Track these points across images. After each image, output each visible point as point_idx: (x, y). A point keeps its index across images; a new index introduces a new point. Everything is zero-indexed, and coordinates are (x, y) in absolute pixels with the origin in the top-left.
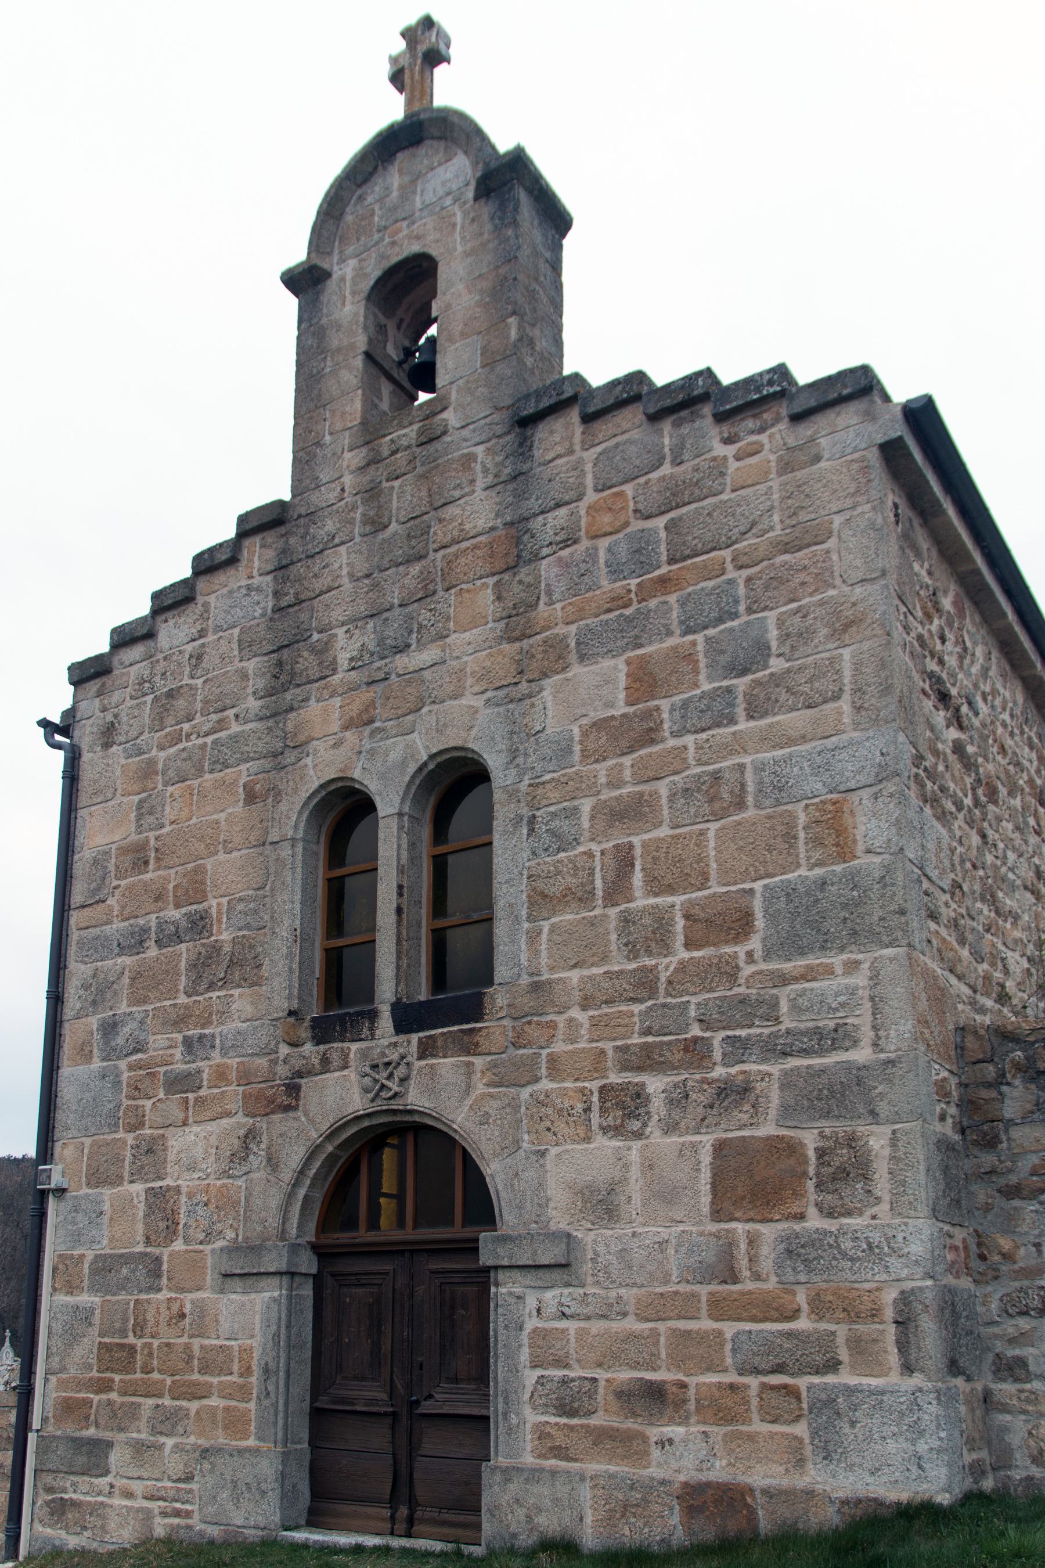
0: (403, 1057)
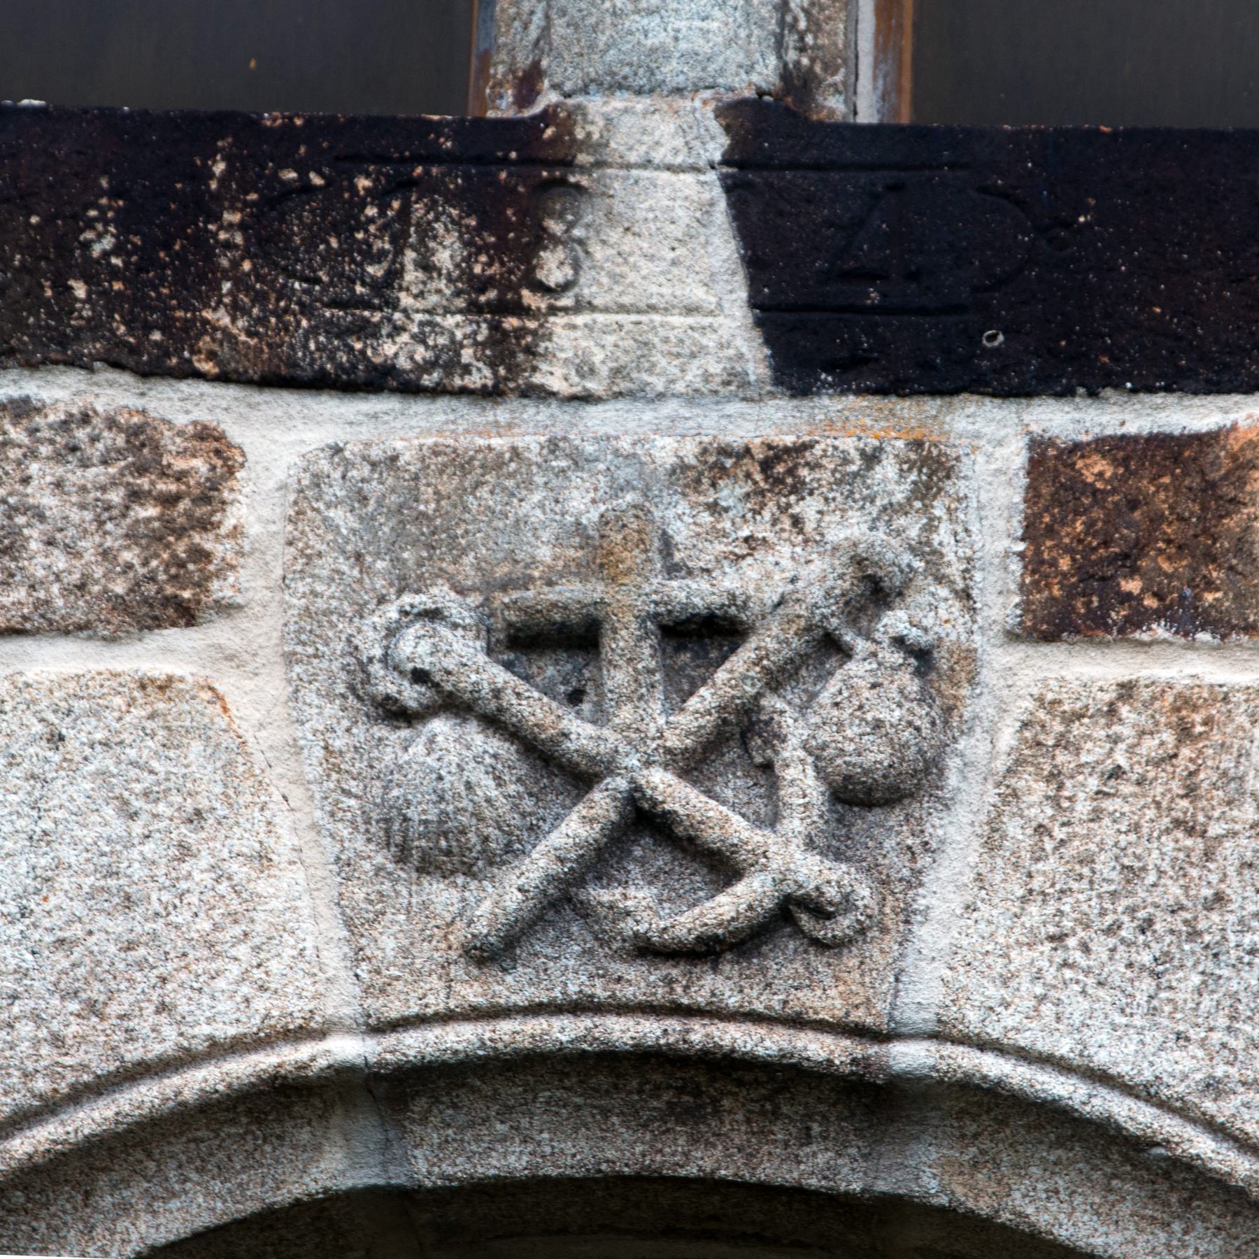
0: (874, 591)
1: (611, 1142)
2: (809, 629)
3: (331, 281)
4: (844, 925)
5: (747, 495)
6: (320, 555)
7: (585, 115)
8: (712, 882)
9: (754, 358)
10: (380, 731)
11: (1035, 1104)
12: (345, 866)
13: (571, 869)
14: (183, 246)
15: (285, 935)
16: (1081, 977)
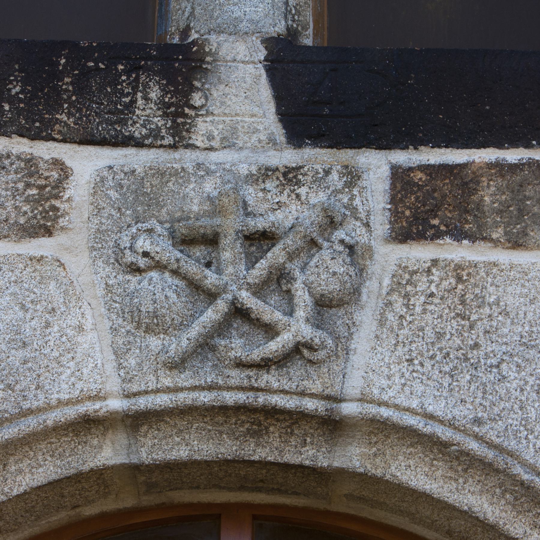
0: (331, 223)
1: (223, 446)
2: (305, 237)
3: (108, 104)
4: (321, 354)
5: (278, 186)
6: (104, 208)
7: (209, 43)
8: (266, 337)
9: (279, 132)
10: (129, 277)
11: (402, 428)
12: (114, 330)
13: (209, 331)
14: (48, 91)
15: (90, 358)
16: (420, 376)
